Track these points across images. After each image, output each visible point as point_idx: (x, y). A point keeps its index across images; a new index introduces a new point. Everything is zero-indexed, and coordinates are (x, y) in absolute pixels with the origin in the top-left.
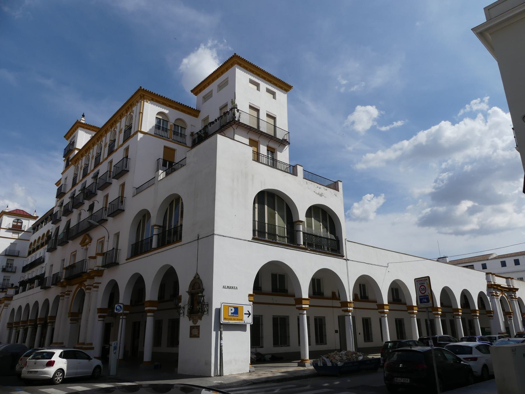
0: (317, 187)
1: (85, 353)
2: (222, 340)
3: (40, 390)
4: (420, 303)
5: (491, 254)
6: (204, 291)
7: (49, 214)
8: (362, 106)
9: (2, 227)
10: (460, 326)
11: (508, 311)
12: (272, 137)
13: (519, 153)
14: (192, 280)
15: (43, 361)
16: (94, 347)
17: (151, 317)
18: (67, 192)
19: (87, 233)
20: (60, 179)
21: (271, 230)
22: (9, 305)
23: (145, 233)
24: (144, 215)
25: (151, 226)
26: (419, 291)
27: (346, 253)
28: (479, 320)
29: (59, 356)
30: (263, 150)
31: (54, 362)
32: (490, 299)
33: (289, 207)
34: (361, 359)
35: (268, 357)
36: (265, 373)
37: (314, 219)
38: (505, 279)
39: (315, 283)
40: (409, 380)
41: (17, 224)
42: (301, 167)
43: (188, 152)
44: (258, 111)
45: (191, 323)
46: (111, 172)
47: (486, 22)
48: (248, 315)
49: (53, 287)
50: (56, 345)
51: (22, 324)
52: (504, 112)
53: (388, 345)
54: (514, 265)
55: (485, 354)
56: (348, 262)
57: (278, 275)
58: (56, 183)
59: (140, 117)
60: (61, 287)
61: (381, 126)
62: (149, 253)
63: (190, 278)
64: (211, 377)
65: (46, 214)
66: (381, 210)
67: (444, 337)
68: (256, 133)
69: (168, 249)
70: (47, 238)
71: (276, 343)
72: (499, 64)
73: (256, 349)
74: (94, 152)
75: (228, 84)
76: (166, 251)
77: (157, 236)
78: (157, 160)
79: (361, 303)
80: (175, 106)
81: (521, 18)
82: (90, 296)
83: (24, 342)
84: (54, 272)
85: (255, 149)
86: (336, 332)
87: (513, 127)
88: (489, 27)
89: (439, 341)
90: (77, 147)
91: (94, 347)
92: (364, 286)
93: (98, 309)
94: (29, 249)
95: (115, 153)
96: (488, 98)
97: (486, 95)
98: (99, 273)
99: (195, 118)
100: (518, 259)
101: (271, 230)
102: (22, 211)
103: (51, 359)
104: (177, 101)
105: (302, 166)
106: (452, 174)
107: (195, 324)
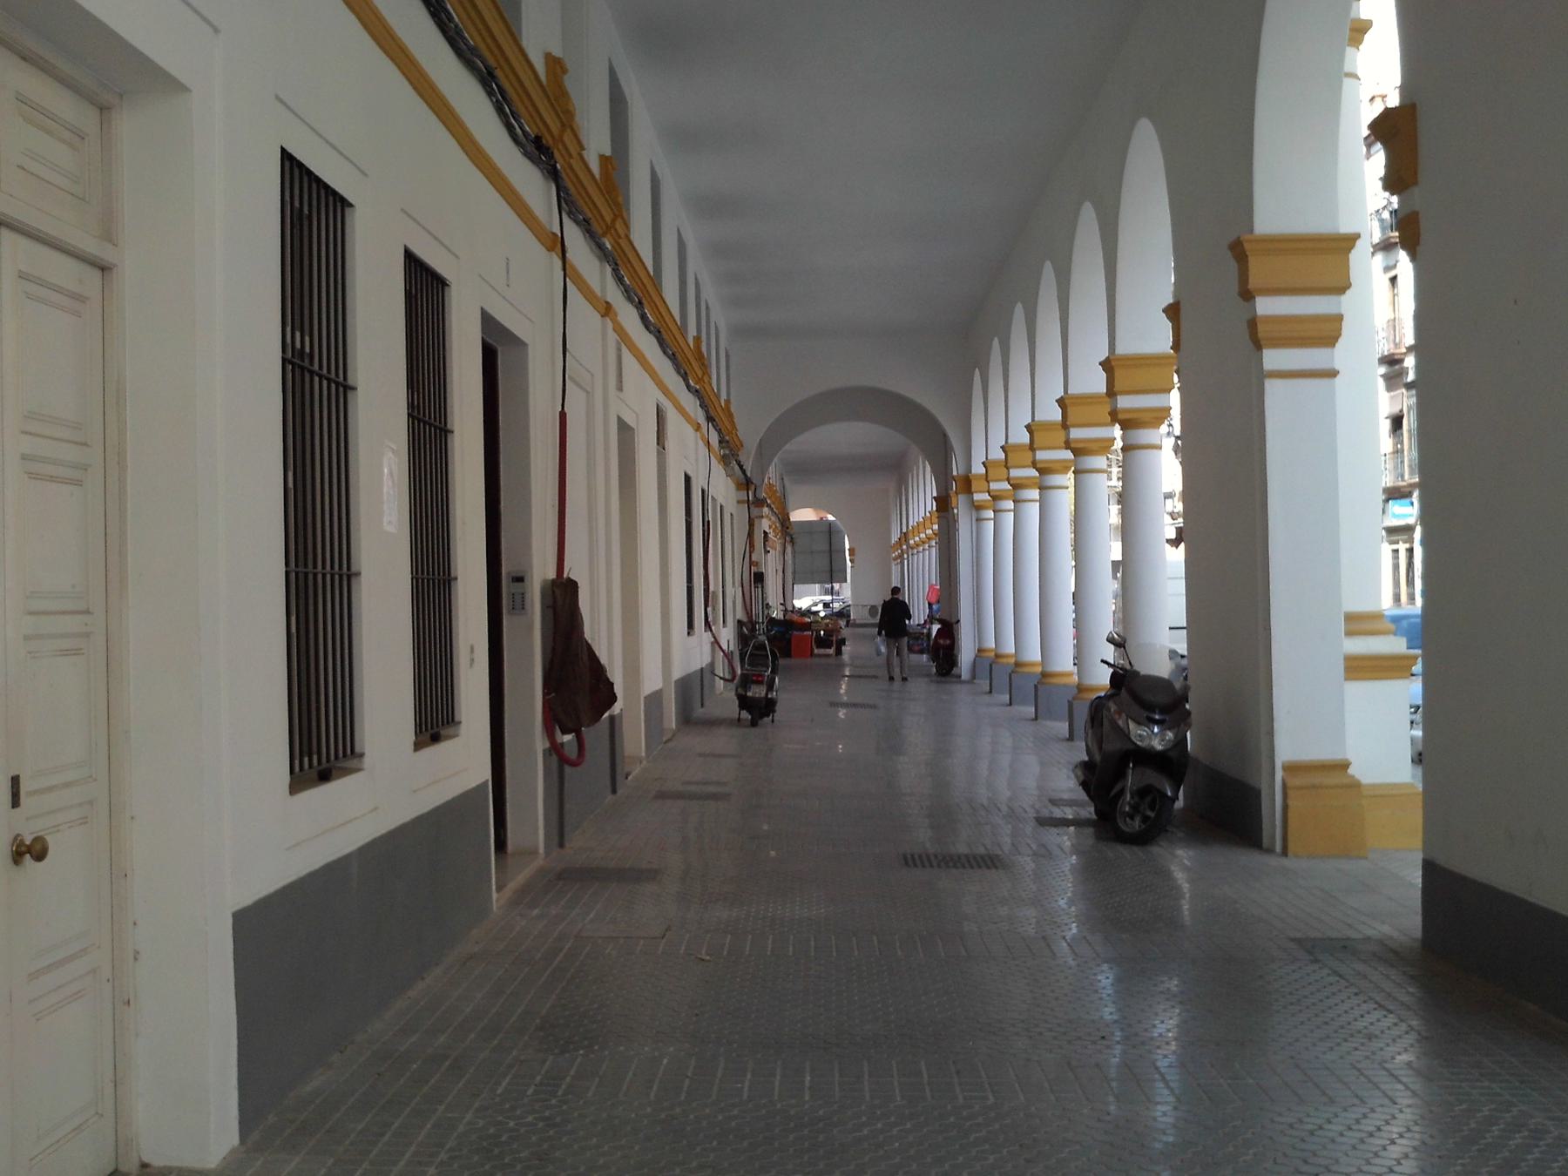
5: (657, 409)
9: (1185, 631)
13: (1171, 324)
14: (585, 297)
19: (1416, 494)
20: (607, 71)
24: (1501, 1088)
25: (673, 684)
27: (604, 347)
30: (572, 1046)
33: (1272, 686)
35: (1395, 561)
36: (707, 308)
38: (1112, 646)
39: (623, 544)
42: (1075, 706)
43: (707, 703)
45: (1188, 682)
46: (851, 665)
53: (1155, 713)
59: (298, 648)
65: (392, 59)
68: (17, 99)
70: (839, 611)
73: (1036, 501)
84: (677, 674)
87: (1351, 771)
92: (84, 302)
93: (1113, 562)
94: (1400, 542)
96: (939, 626)
97: (1143, 826)
99: (1369, 123)
100: (1165, 311)
106: (1188, 923)
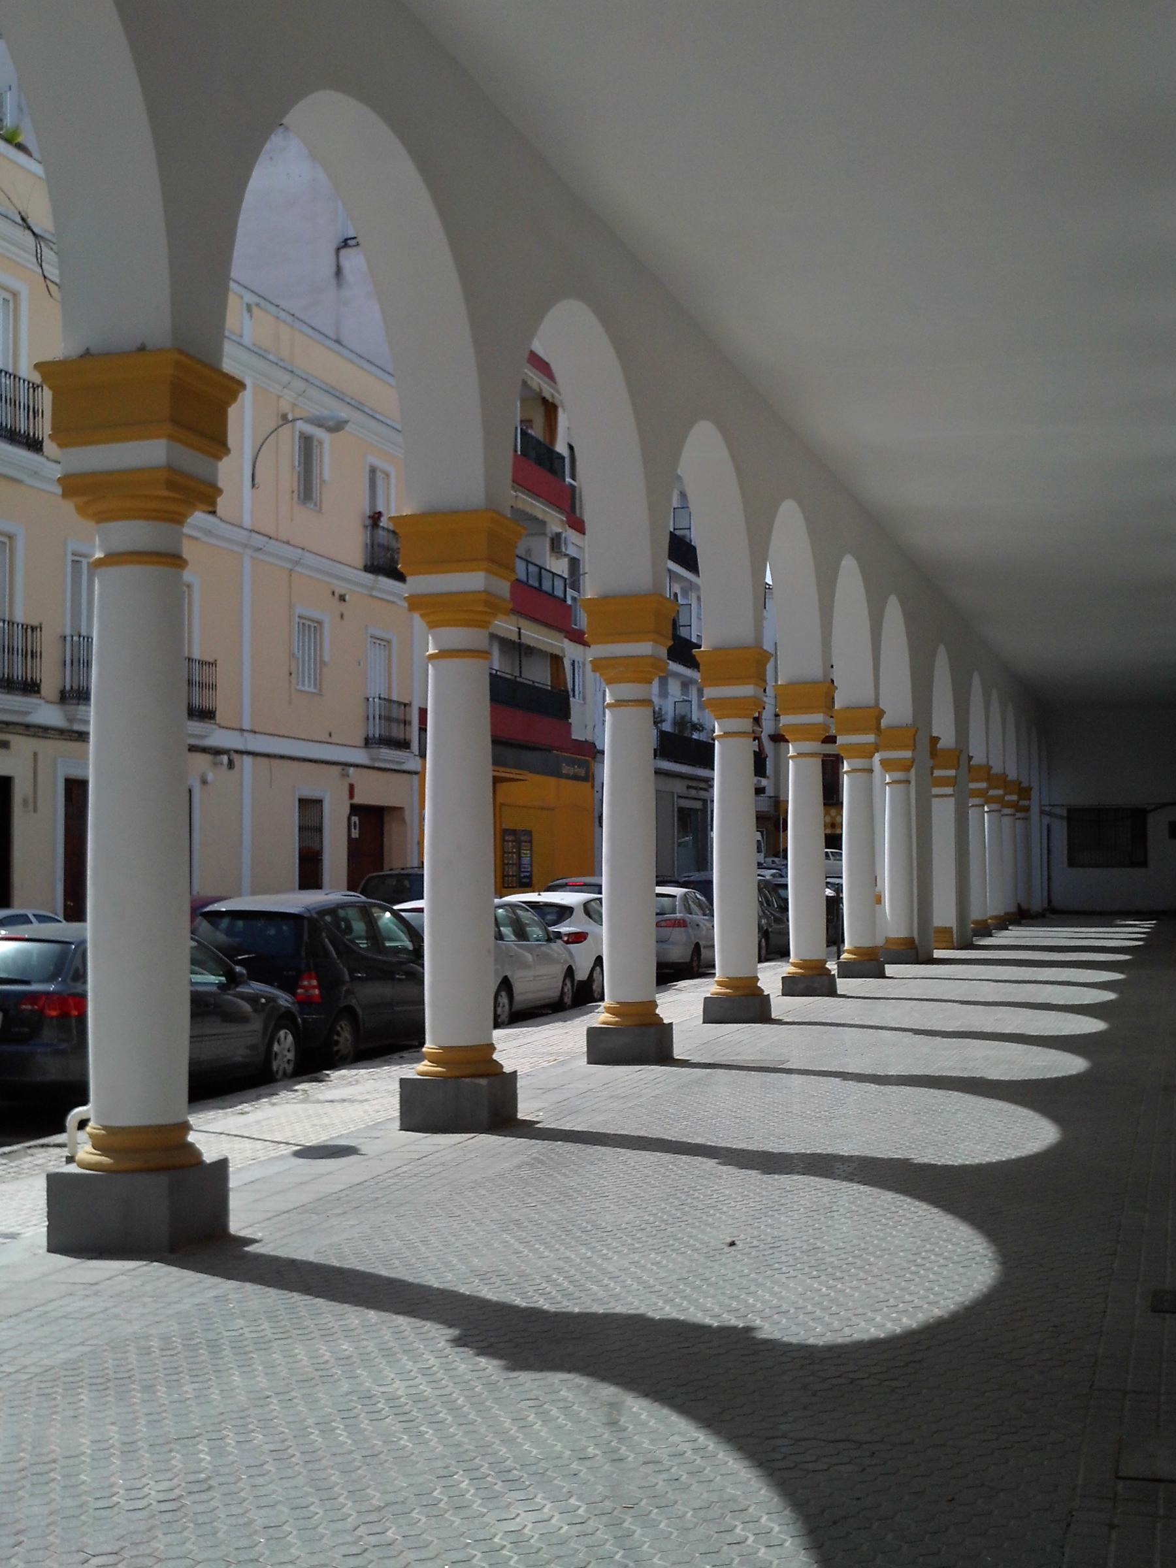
0: (740, 1245)
2: (655, 749)
3: (888, 917)
4: (422, 898)
7: (549, 385)
12: (514, 642)
16: (764, 788)
17: (872, 693)
18: (555, 580)
21: (197, 699)
22: (376, 731)
23: (715, 834)
29: (755, 772)
31: (37, 366)
34: (276, 141)
40: (357, 836)
44: (331, 430)
48: (543, 570)
49: (1041, 821)
50: (630, 703)
51: (611, 1545)
52: (656, 1401)
56: (335, 338)
58: (757, 959)
61: (241, 975)
64: (956, 776)
67: (944, 945)
69: (39, 763)
74: (1015, 969)
81: (297, 632)
83: (702, 785)
86: (539, 895)
88: (400, 751)
91: (764, 788)
95: (217, 712)
98: (149, 1313)
101: (197, 699)
103: (563, 458)
105: (59, 463)
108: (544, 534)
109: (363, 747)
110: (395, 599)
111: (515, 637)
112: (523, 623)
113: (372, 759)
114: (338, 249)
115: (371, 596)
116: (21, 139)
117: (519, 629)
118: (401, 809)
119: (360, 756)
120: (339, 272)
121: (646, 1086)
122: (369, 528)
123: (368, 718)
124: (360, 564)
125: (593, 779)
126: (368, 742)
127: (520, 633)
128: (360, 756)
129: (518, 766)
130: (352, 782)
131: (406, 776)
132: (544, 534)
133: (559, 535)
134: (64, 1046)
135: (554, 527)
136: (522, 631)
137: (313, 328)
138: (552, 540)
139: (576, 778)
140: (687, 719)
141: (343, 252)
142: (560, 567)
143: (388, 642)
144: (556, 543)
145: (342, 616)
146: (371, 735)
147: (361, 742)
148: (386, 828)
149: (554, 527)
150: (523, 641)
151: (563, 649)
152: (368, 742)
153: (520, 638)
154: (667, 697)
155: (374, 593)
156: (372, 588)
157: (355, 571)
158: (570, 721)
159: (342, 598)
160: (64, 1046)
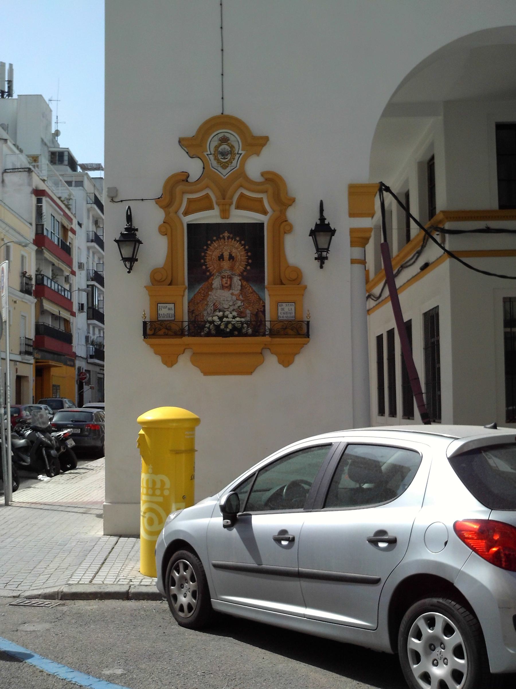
1: (367, 336)
6: (265, 170)
8: (13, 69)
10: (268, 237)
11: (78, 465)
15: (267, 227)
23: (442, 615)
25: (196, 581)
26: (282, 221)
28: (4, 77)
32: (392, 499)
37: (54, 242)
41: (263, 321)
47: (313, 237)
54: (387, 330)
55: (213, 497)
57: (41, 205)
58: (439, 308)
60: (75, 353)
62: (451, 401)
63: (181, 154)
66: (229, 238)
71: (211, 208)
72: (235, 638)
75: (251, 373)
76: (221, 82)
77: (426, 394)
78: (308, 322)
79: (313, 242)
80: (49, 307)
82: (116, 503)
85: (364, 249)
88: (355, 506)
89: (207, 196)
90: (60, 147)
102: (232, 496)
104: (27, 271)
107: (348, 464)
108: (63, 275)
109: (19, 355)
110: (27, 302)
111: (58, 314)
112: (60, 309)
113: (22, 359)
114: (3, 173)
115: (22, 301)
116: (70, 207)
117: (59, 311)
118: (27, 377)
119: (18, 358)
120: (3, 181)
121: (64, 489)
122: (22, 277)
123: (21, 344)
124: (19, 289)
125: (75, 366)
126: (21, 353)
127: (60, 313)
128: (18, 358)
129: (58, 361)
130: (17, 367)
131: (29, 365)
132: (63, 275)
133: (68, 276)
134: (95, 437)
135: (67, 273)
136: (60, 312)
137: (9, 208)
138: (65, 278)
139: (71, 366)
140: (102, 344)
141: (5, 174)
142: (67, 287)
143: (25, 317)
144: (67, 279)
145: (15, 308)
146: (22, 350)
147: (19, 353)
148: (22, 384)
149: (67, 273)
150: (61, 315)
151: (70, 318)
152: (21, 353)
153: (60, 315)
154: (94, 335)
155: (23, 300)
156: (22, 298)
157: (18, 292)
158: (72, 345)
159: (15, 302)
160: (95, 437)
